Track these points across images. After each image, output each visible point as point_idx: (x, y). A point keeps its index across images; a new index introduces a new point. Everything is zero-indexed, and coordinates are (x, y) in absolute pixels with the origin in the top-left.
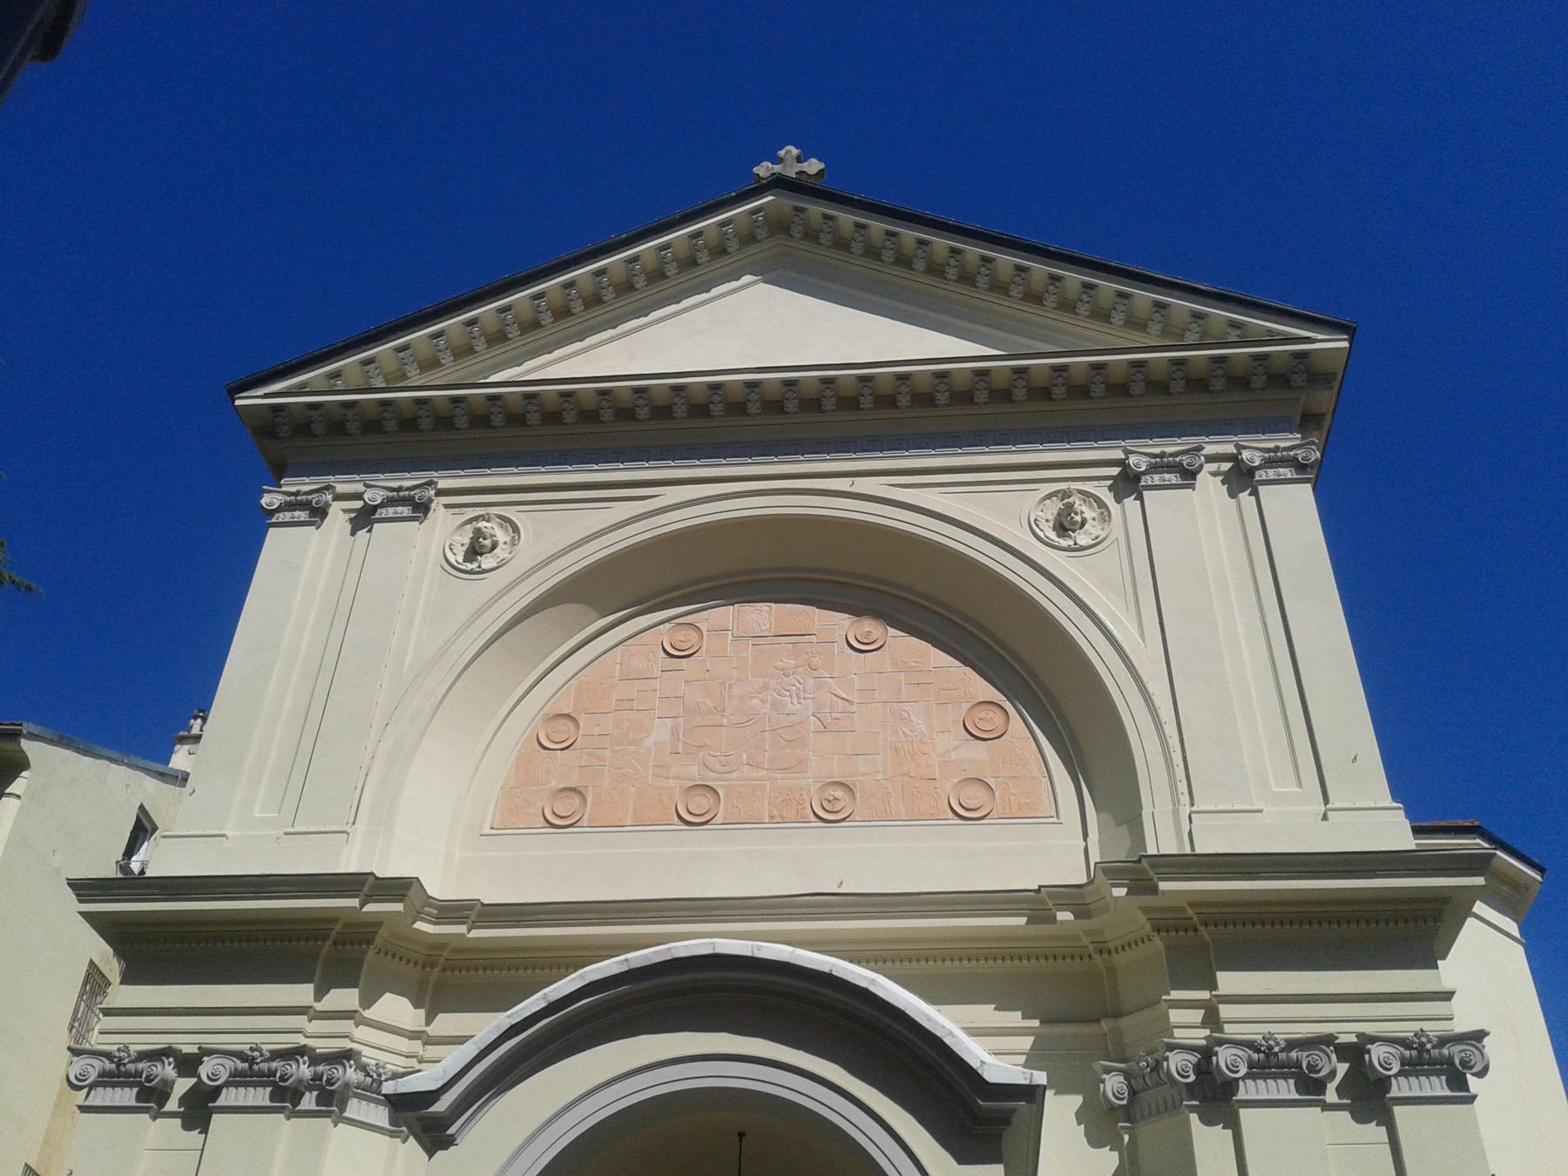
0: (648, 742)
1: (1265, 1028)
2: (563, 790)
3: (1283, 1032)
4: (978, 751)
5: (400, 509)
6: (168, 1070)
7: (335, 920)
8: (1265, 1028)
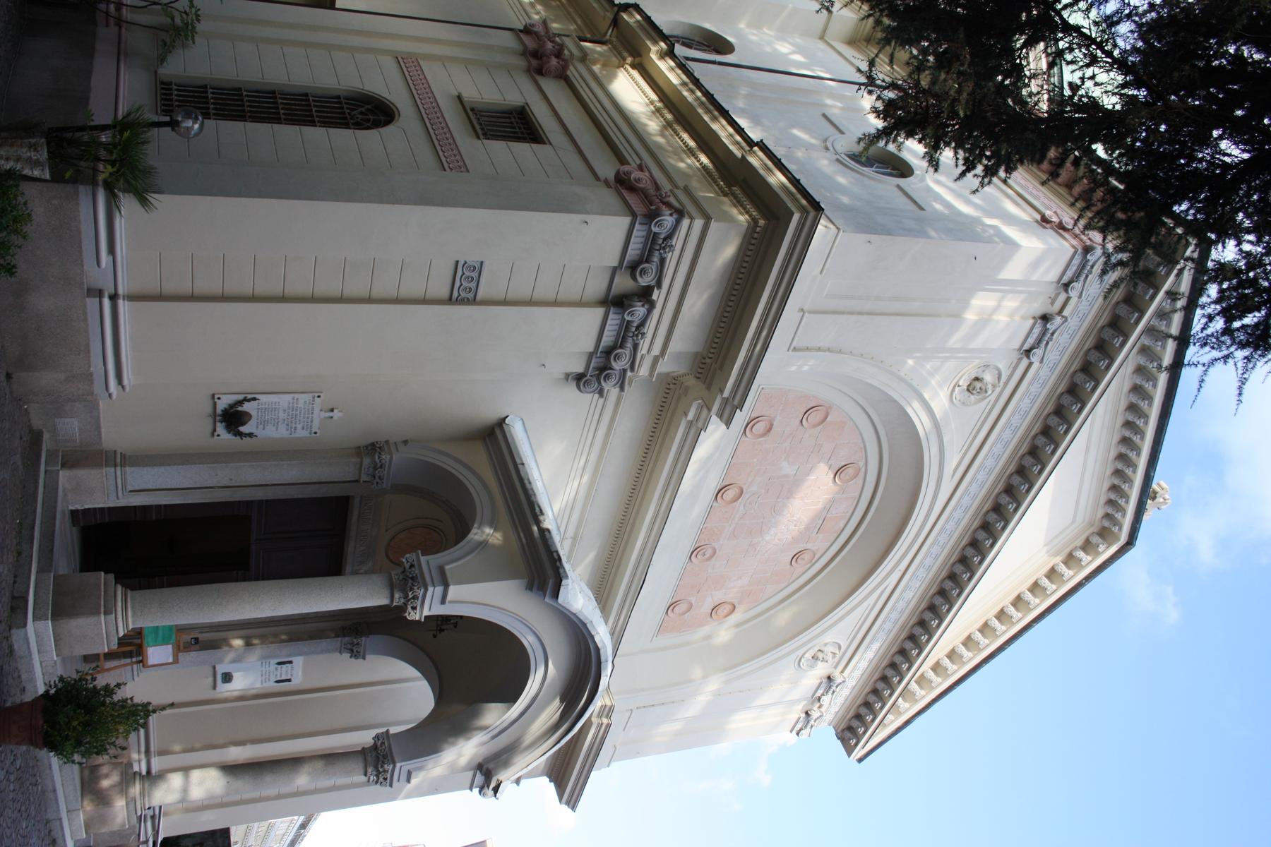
0: (785, 464)
1: (649, 335)
2: (772, 425)
3: (672, 259)
4: (707, 608)
5: (1074, 268)
6: (644, 281)
7: (721, 368)
8: (649, 335)
